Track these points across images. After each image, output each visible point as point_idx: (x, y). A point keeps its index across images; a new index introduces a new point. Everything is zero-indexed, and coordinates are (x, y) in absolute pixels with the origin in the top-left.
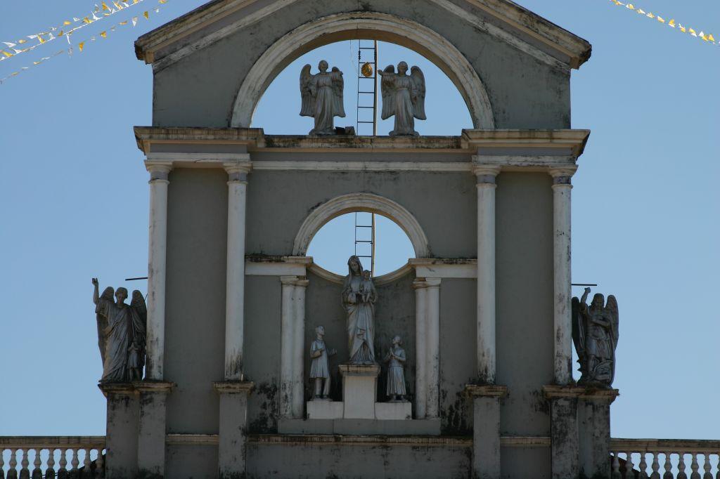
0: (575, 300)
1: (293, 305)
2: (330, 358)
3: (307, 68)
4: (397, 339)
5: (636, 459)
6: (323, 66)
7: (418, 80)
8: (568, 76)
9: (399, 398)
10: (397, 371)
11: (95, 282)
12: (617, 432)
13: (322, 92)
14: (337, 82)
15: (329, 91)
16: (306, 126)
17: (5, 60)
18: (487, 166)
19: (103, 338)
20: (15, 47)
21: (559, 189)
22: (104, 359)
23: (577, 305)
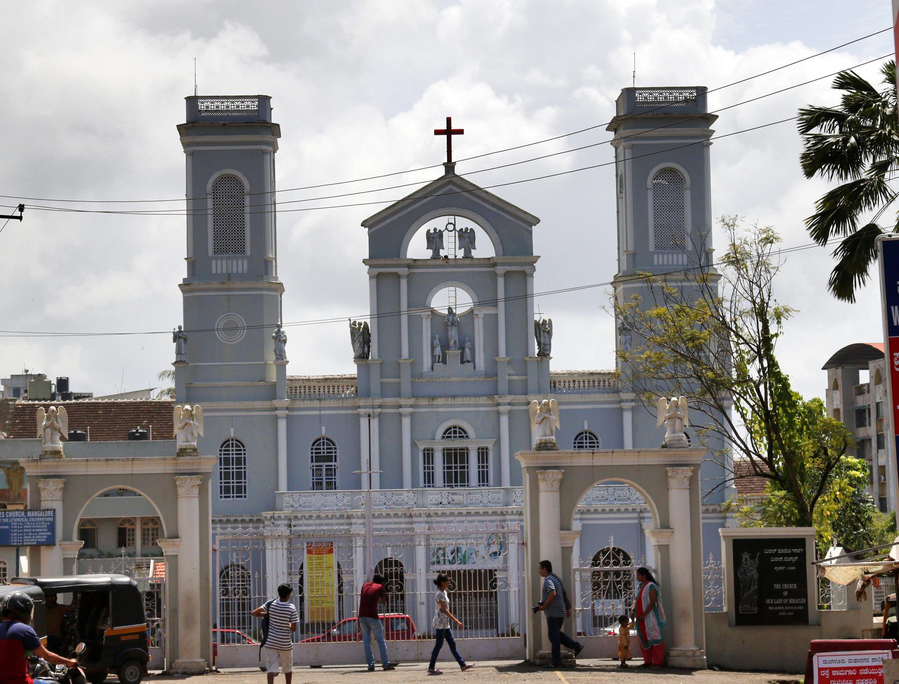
0: (536, 321)
2: (441, 346)
3: (428, 231)
4: (467, 338)
6: (435, 229)
7: (472, 233)
9: (468, 362)
10: (467, 351)
11: (350, 320)
13: (435, 240)
15: (438, 240)
18: (500, 270)
21: (529, 279)
22: (354, 350)
23: (537, 324)
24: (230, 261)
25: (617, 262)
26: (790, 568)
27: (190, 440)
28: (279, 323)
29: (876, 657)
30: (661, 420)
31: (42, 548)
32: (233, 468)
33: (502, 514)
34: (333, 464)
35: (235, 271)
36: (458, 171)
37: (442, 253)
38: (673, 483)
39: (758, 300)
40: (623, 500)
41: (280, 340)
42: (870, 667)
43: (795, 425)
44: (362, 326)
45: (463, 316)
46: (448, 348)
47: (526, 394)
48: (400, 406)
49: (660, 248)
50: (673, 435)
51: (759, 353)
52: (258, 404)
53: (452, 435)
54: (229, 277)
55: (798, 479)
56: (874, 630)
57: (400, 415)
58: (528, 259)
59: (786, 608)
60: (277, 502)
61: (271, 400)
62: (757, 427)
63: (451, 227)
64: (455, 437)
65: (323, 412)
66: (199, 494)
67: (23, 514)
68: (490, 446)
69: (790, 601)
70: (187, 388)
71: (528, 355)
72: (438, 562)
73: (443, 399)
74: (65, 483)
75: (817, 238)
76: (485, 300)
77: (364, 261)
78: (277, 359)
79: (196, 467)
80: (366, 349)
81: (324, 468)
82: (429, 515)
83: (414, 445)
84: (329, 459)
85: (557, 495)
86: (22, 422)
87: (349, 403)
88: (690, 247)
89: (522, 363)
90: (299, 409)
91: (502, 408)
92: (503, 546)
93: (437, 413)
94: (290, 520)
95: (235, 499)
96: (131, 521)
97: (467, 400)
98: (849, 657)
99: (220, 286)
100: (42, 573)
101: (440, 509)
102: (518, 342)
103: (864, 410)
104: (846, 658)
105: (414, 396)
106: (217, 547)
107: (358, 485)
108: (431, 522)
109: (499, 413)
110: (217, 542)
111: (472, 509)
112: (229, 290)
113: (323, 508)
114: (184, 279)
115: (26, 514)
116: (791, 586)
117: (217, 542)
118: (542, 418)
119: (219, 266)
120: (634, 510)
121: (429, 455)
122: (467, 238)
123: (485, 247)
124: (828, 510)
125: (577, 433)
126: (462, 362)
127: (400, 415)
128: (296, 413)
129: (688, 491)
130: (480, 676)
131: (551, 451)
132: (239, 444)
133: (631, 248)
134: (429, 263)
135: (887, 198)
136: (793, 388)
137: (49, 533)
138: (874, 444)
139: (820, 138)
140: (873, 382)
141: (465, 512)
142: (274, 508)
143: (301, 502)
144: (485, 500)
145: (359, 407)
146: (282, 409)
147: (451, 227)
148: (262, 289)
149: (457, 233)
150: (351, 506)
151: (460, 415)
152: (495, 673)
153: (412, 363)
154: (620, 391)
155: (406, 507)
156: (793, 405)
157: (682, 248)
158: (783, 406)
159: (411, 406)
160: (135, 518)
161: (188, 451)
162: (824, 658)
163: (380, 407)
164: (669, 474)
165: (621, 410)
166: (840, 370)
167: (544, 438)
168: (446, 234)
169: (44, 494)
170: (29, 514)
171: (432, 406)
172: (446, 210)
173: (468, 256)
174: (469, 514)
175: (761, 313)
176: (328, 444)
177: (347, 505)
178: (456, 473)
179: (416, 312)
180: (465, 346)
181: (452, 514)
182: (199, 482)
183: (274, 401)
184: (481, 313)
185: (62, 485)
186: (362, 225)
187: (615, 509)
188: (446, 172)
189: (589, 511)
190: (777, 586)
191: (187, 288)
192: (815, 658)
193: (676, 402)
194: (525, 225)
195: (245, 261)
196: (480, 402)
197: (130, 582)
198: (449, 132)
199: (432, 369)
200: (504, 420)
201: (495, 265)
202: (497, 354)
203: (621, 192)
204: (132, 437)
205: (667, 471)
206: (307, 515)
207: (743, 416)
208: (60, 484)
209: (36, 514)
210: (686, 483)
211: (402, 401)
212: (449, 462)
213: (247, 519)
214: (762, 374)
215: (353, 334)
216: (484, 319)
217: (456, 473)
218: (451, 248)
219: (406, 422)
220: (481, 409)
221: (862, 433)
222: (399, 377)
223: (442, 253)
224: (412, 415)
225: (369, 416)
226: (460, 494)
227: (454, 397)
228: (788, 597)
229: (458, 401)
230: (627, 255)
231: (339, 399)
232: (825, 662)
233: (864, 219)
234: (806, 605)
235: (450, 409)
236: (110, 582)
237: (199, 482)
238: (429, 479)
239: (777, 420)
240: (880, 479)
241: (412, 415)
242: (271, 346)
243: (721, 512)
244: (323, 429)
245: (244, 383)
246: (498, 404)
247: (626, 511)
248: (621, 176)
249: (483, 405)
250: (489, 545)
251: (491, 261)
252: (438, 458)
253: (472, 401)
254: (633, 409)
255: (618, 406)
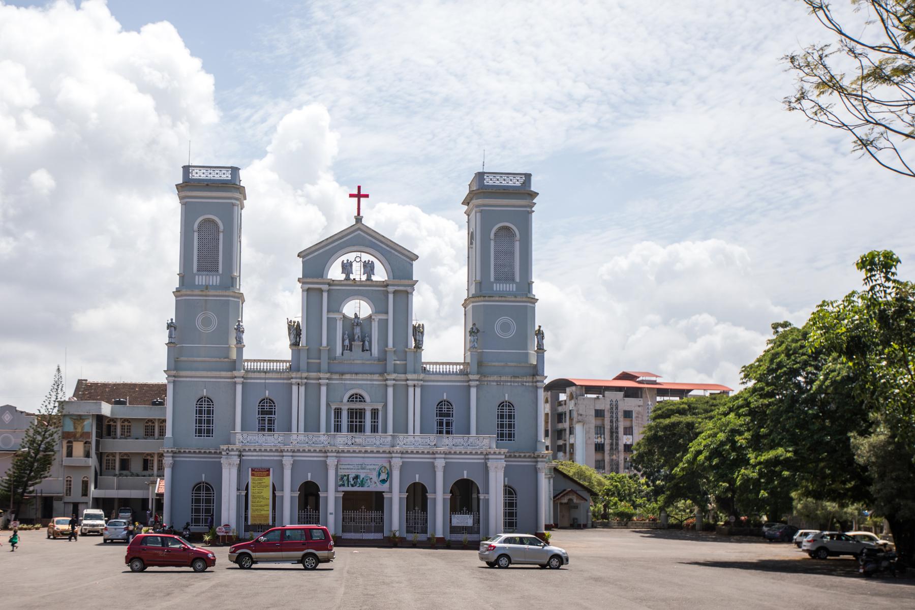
1: (339, 325)
5: (428, 366)
6: (348, 260)
8: (412, 265)
9: (367, 350)
10: (367, 343)
12: (423, 361)
14: (351, 264)
16: (342, 277)
17: (788, 446)
18: (391, 289)
19: (290, 334)
20: (817, 466)
21: (410, 296)
23: (414, 327)
24: (208, 277)
25: (467, 291)
28: (240, 319)
33: (390, 453)
34: (273, 416)
35: (211, 284)
40: (474, 446)
41: (239, 331)
44: (296, 324)
46: (354, 340)
47: (405, 373)
48: (320, 379)
49: (497, 280)
52: (224, 374)
53: (355, 400)
54: (207, 287)
60: (232, 439)
61: (231, 371)
63: (358, 260)
64: (356, 401)
65: (267, 381)
68: (380, 408)
70: (175, 361)
71: (407, 348)
72: (344, 485)
73: (349, 375)
76: (380, 307)
78: (237, 343)
80: (298, 339)
81: (267, 419)
82: (338, 452)
83: (328, 405)
86: (90, 393)
88: (517, 279)
89: (403, 353)
90: (251, 378)
91: (389, 383)
92: (389, 474)
94: (240, 451)
95: (205, 438)
96: (152, 455)
97: (365, 377)
99: (200, 293)
101: (346, 448)
102: (401, 338)
103: (562, 414)
107: (290, 430)
108: (340, 457)
109: (386, 386)
111: (369, 448)
112: (206, 296)
113: (264, 444)
114: (177, 288)
120: (482, 453)
121: (338, 412)
122: (369, 268)
123: (380, 275)
125: (439, 401)
126: (363, 350)
127: (320, 385)
128: (249, 381)
132: (210, 400)
133: (478, 278)
134: (342, 282)
138: (568, 432)
140: (568, 399)
141: (363, 451)
142: (229, 443)
143: (248, 440)
144: (378, 443)
145: (292, 378)
147: (358, 260)
149: (362, 264)
150: (283, 443)
151: (360, 386)
153: (329, 350)
155: (322, 445)
157: (513, 280)
159: (327, 379)
160: (154, 453)
165: (469, 386)
166: (549, 393)
168: (354, 264)
171: (342, 379)
173: (369, 279)
174: (366, 452)
177: (281, 443)
178: (356, 425)
179: (332, 315)
180: (365, 340)
181: (354, 452)
183: (234, 372)
184: (377, 318)
186: (298, 256)
187: (468, 452)
189: (450, 453)
191: (178, 294)
195: (218, 277)
196: (374, 378)
198: (359, 196)
199: (342, 354)
200: (390, 391)
201: (387, 286)
202: (387, 346)
203: (472, 244)
204: (154, 404)
206: (252, 449)
211: (322, 375)
213: (213, 451)
216: (378, 322)
217: (356, 425)
218: (358, 274)
219: (324, 389)
220: (375, 383)
221: (560, 426)
222: (320, 359)
223: (352, 277)
225: (299, 384)
226: (359, 438)
227: (356, 374)
229: (360, 377)
230: (476, 283)
235: (353, 382)
240: (570, 451)
241: (327, 385)
242: (233, 335)
243: (534, 457)
244: (267, 392)
245: (214, 359)
246: (387, 380)
249: (376, 380)
250: (379, 474)
251: (385, 283)
252: (345, 415)
253: (369, 377)
254: (477, 386)
255: (467, 384)
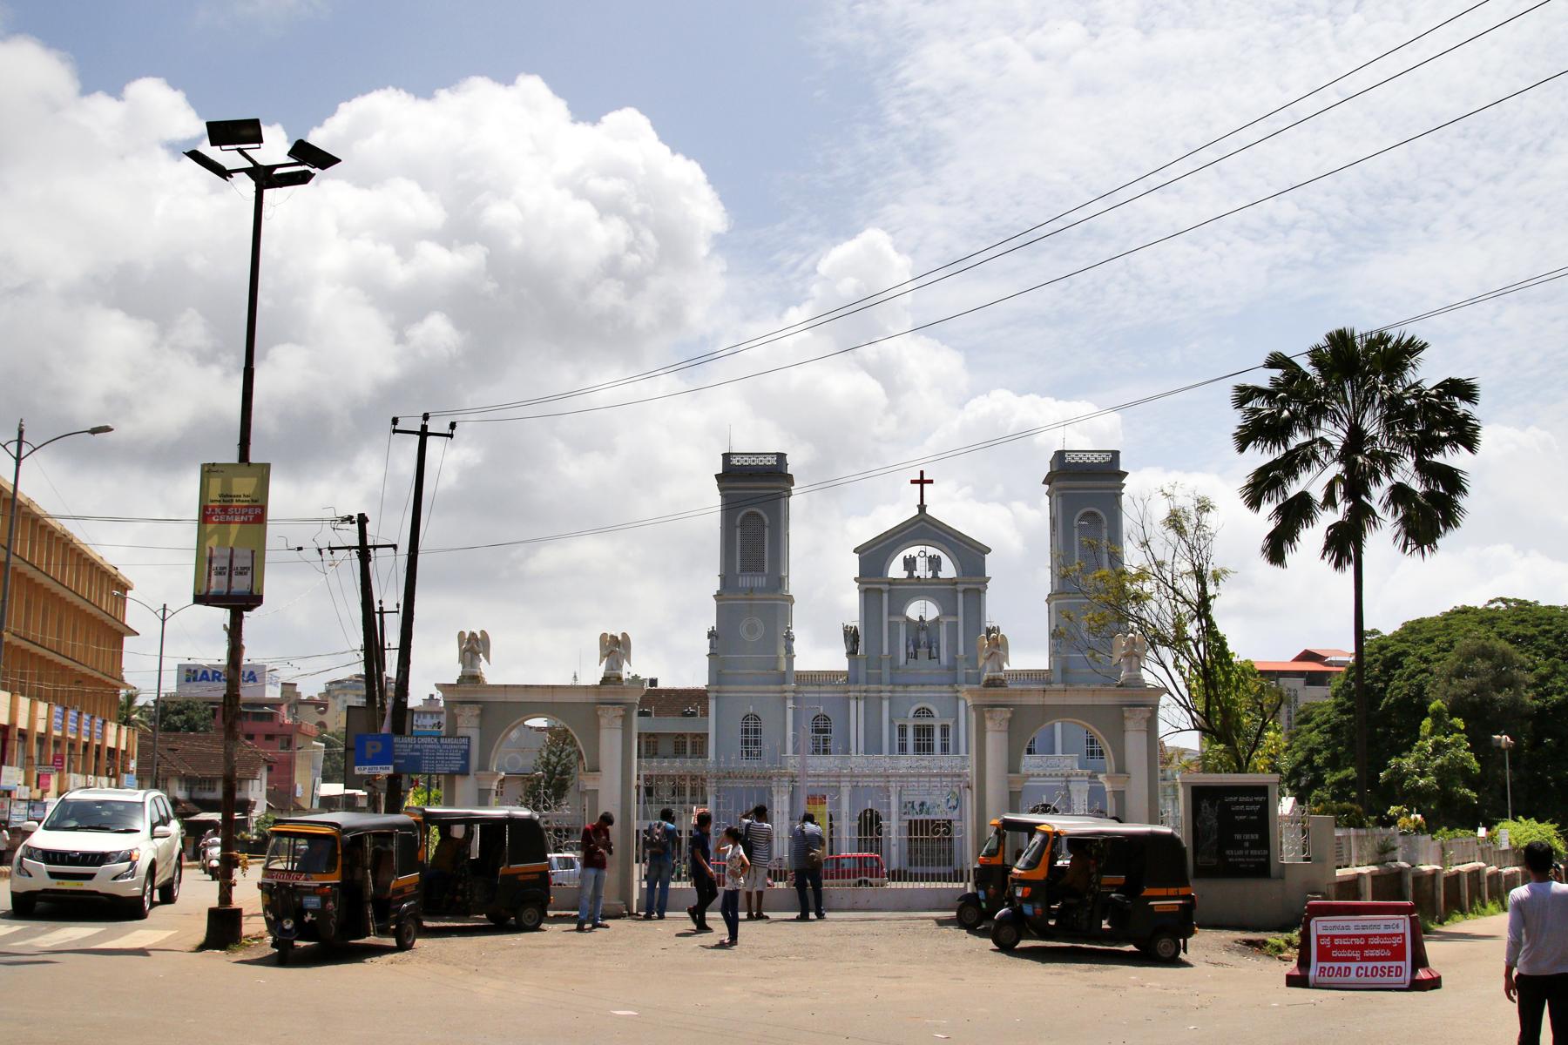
10: (934, 650)
18: (960, 587)
26: (1252, 818)
27: (615, 668)
29: (1390, 922)
30: (1117, 656)
31: (457, 777)
32: (751, 737)
34: (829, 735)
36: (928, 511)
37: (916, 574)
38: (1130, 724)
39: (1197, 563)
42: (1382, 936)
43: (1232, 682)
45: (930, 622)
46: (919, 647)
48: (881, 692)
50: (1129, 673)
51: (1198, 612)
52: (772, 688)
54: (752, 589)
55: (1234, 733)
56: (1337, 883)
57: (881, 698)
58: (982, 579)
59: (1247, 860)
61: (781, 684)
62: (1194, 684)
63: (922, 554)
65: (821, 695)
66: (623, 726)
67: (436, 740)
68: (950, 724)
69: (1252, 852)
74: (482, 710)
75: (1251, 506)
76: (948, 609)
77: (856, 579)
78: (787, 653)
79: (620, 697)
80: (855, 647)
83: (891, 722)
84: (825, 731)
85: (1005, 736)
87: (842, 688)
93: (910, 697)
98: (1356, 923)
100: (456, 804)
104: (1352, 924)
105: (892, 683)
106: (642, 783)
110: (642, 778)
115: (439, 741)
116: (1253, 837)
117: (642, 778)
118: (989, 653)
119: (745, 581)
121: (903, 730)
122: (934, 563)
123: (948, 570)
124: (1262, 764)
126: (930, 658)
129: (1145, 734)
130: (917, 931)
131: (1000, 688)
132: (757, 718)
134: (905, 581)
135: (1320, 465)
136: (1230, 648)
137: (463, 762)
139: (1254, 411)
145: (849, 691)
146: (790, 692)
147: (922, 554)
148: (776, 599)
151: (928, 699)
152: (934, 927)
154: (1053, 683)
156: (1230, 663)
158: (1220, 664)
159: (890, 692)
161: (612, 679)
162: (1325, 924)
163: (865, 691)
164: (1126, 715)
167: (992, 674)
169: (460, 721)
170: (442, 741)
171: (906, 692)
172: (919, 541)
173: (935, 576)
175: (1200, 575)
176: (825, 720)
182: (622, 713)
185: (477, 712)
187: (1048, 774)
188: (919, 512)
190: (1238, 837)
192: (1313, 923)
193: (1133, 639)
194: (979, 553)
195: (764, 579)
197: (531, 816)
198: (922, 482)
201: (956, 583)
204: (685, 714)
205: (1123, 712)
207: (1182, 673)
208: (476, 710)
209: (449, 741)
210: (1144, 726)
211: (883, 688)
212: (919, 735)
214: (1201, 632)
215: (845, 635)
218: (922, 570)
219: (886, 704)
223: (916, 574)
224: (890, 698)
226: (925, 760)
227: (923, 685)
228: (1251, 848)
229: (927, 688)
231: (833, 685)
232: (1325, 928)
233: (1293, 489)
234: (1268, 857)
236: (508, 815)
237: (622, 713)
238: (903, 749)
239: (1215, 677)
241: (890, 698)
242: (782, 643)
245: (761, 672)
247: (1057, 775)
248: (1054, 519)
253: (937, 688)
